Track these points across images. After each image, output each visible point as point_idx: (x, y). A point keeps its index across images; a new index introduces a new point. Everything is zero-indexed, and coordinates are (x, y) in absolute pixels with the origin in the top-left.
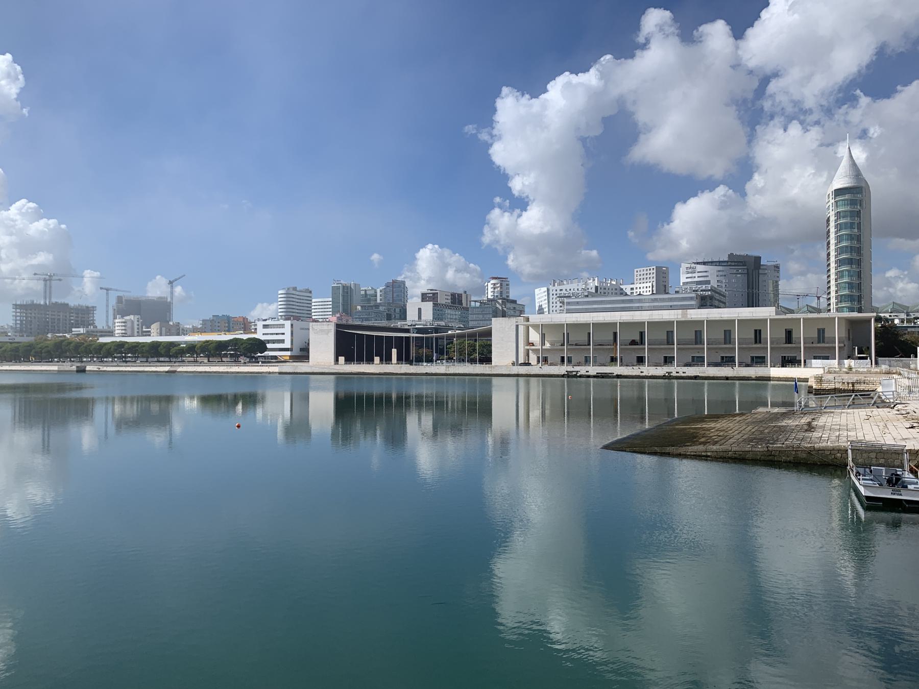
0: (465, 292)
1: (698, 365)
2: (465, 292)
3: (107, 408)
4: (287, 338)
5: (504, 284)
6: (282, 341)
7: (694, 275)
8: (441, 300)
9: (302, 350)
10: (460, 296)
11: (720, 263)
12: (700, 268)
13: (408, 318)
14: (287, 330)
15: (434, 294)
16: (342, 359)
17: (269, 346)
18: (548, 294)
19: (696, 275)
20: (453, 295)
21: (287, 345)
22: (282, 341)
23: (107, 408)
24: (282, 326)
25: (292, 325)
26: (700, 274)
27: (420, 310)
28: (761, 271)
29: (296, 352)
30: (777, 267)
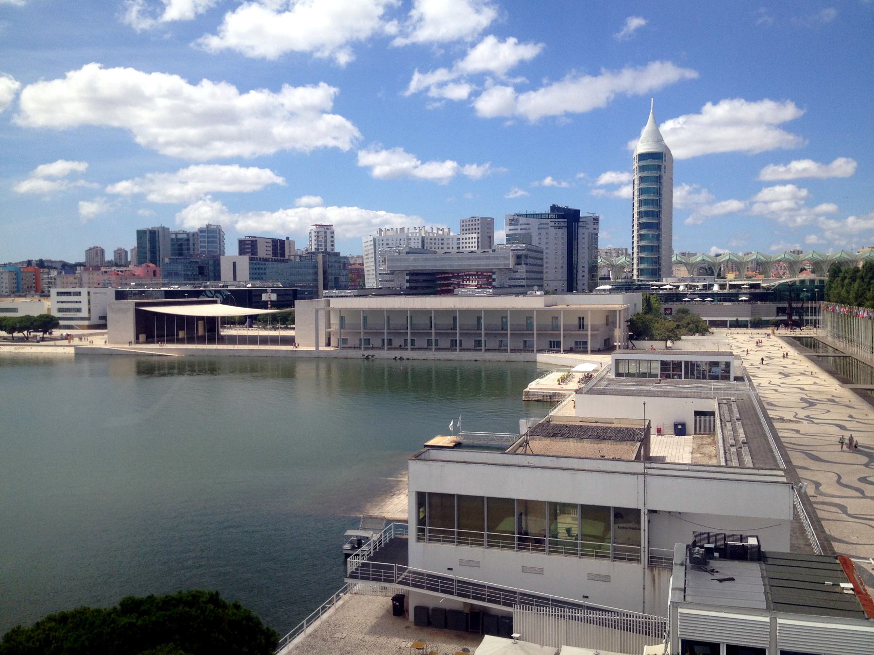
0: (288, 238)
1: (553, 352)
2: (288, 238)
3: (317, 369)
4: (84, 307)
5: (328, 232)
6: (79, 310)
7: (517, 227)
8: (263, 252)
9: (101, 318)
10: (282, 243)
11: (540, 216)
12: (522, 220)
13: (223, 278)
14: (84, 298)
15: (252, 241)
16: (142, 337)
17: (61, 323)
18: (375, 247)
19: (518, 227)
20: (275, 241)
21: (84, 313)
22: (79, 310)
23: (317, 369)
24: (79, 294)
25: (89, 293)
26: (523, 227)
27: (234, 263)
28: (580, 224)
29: (95, 320)
30: (596, 220)
